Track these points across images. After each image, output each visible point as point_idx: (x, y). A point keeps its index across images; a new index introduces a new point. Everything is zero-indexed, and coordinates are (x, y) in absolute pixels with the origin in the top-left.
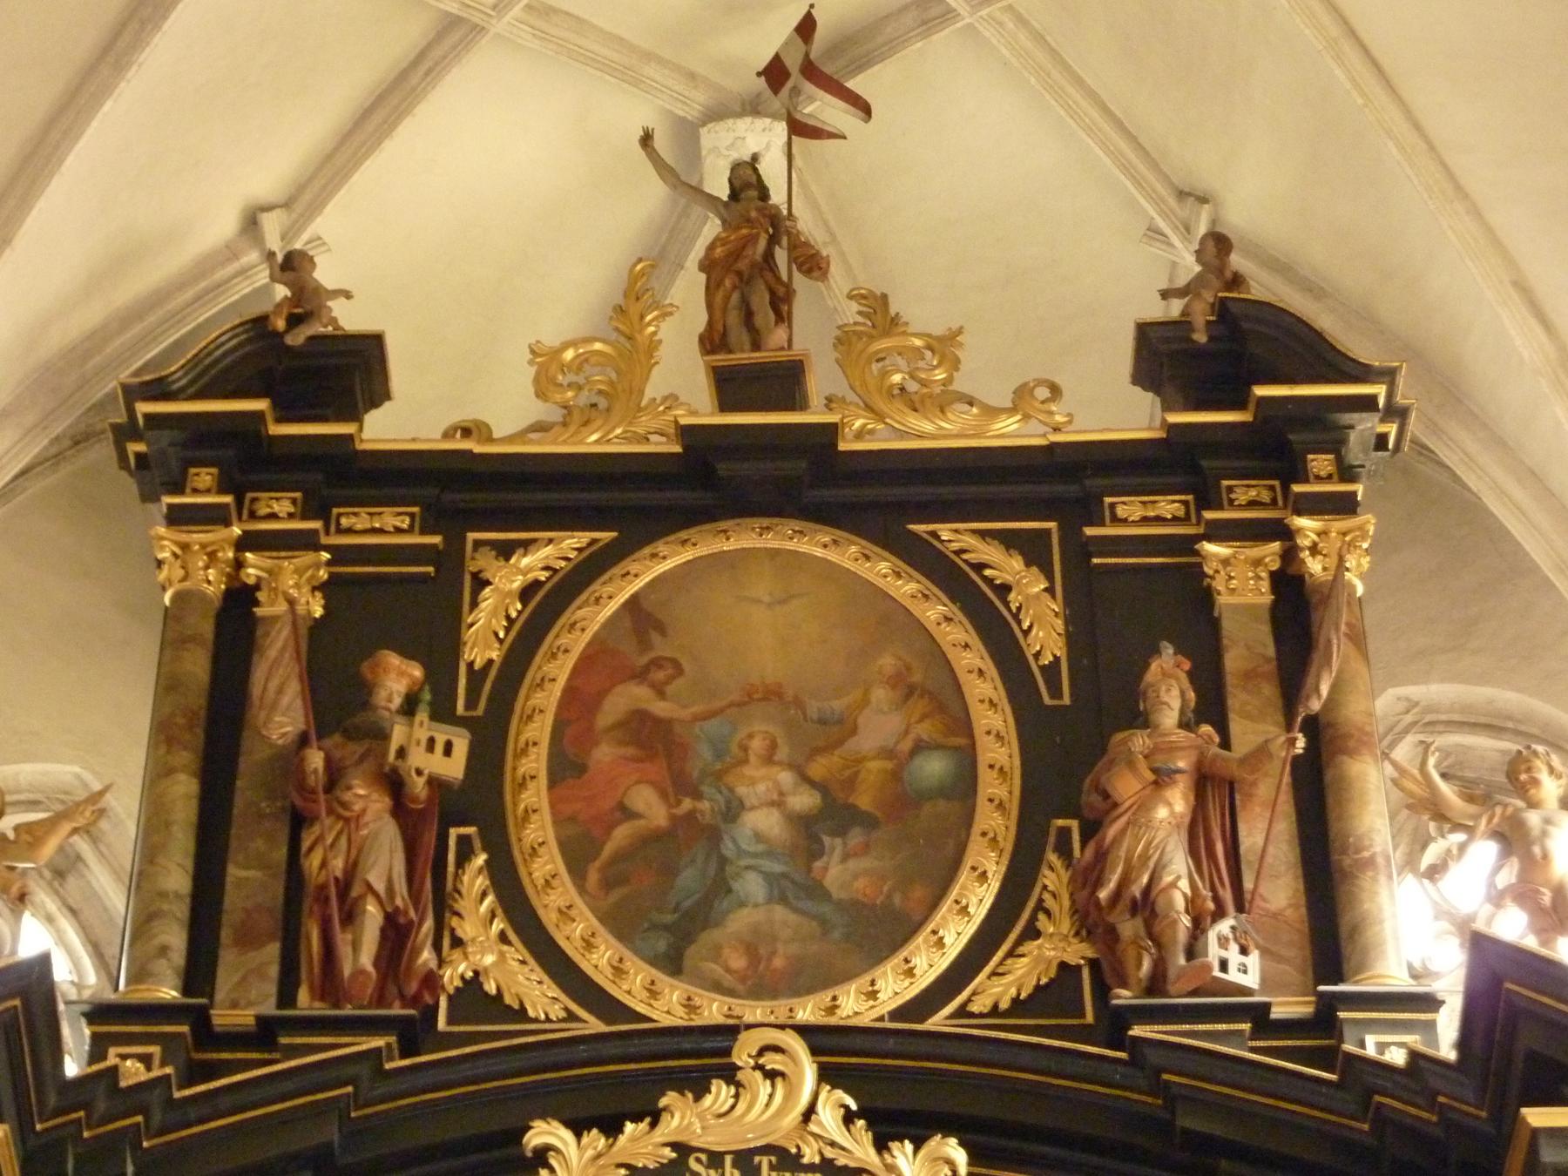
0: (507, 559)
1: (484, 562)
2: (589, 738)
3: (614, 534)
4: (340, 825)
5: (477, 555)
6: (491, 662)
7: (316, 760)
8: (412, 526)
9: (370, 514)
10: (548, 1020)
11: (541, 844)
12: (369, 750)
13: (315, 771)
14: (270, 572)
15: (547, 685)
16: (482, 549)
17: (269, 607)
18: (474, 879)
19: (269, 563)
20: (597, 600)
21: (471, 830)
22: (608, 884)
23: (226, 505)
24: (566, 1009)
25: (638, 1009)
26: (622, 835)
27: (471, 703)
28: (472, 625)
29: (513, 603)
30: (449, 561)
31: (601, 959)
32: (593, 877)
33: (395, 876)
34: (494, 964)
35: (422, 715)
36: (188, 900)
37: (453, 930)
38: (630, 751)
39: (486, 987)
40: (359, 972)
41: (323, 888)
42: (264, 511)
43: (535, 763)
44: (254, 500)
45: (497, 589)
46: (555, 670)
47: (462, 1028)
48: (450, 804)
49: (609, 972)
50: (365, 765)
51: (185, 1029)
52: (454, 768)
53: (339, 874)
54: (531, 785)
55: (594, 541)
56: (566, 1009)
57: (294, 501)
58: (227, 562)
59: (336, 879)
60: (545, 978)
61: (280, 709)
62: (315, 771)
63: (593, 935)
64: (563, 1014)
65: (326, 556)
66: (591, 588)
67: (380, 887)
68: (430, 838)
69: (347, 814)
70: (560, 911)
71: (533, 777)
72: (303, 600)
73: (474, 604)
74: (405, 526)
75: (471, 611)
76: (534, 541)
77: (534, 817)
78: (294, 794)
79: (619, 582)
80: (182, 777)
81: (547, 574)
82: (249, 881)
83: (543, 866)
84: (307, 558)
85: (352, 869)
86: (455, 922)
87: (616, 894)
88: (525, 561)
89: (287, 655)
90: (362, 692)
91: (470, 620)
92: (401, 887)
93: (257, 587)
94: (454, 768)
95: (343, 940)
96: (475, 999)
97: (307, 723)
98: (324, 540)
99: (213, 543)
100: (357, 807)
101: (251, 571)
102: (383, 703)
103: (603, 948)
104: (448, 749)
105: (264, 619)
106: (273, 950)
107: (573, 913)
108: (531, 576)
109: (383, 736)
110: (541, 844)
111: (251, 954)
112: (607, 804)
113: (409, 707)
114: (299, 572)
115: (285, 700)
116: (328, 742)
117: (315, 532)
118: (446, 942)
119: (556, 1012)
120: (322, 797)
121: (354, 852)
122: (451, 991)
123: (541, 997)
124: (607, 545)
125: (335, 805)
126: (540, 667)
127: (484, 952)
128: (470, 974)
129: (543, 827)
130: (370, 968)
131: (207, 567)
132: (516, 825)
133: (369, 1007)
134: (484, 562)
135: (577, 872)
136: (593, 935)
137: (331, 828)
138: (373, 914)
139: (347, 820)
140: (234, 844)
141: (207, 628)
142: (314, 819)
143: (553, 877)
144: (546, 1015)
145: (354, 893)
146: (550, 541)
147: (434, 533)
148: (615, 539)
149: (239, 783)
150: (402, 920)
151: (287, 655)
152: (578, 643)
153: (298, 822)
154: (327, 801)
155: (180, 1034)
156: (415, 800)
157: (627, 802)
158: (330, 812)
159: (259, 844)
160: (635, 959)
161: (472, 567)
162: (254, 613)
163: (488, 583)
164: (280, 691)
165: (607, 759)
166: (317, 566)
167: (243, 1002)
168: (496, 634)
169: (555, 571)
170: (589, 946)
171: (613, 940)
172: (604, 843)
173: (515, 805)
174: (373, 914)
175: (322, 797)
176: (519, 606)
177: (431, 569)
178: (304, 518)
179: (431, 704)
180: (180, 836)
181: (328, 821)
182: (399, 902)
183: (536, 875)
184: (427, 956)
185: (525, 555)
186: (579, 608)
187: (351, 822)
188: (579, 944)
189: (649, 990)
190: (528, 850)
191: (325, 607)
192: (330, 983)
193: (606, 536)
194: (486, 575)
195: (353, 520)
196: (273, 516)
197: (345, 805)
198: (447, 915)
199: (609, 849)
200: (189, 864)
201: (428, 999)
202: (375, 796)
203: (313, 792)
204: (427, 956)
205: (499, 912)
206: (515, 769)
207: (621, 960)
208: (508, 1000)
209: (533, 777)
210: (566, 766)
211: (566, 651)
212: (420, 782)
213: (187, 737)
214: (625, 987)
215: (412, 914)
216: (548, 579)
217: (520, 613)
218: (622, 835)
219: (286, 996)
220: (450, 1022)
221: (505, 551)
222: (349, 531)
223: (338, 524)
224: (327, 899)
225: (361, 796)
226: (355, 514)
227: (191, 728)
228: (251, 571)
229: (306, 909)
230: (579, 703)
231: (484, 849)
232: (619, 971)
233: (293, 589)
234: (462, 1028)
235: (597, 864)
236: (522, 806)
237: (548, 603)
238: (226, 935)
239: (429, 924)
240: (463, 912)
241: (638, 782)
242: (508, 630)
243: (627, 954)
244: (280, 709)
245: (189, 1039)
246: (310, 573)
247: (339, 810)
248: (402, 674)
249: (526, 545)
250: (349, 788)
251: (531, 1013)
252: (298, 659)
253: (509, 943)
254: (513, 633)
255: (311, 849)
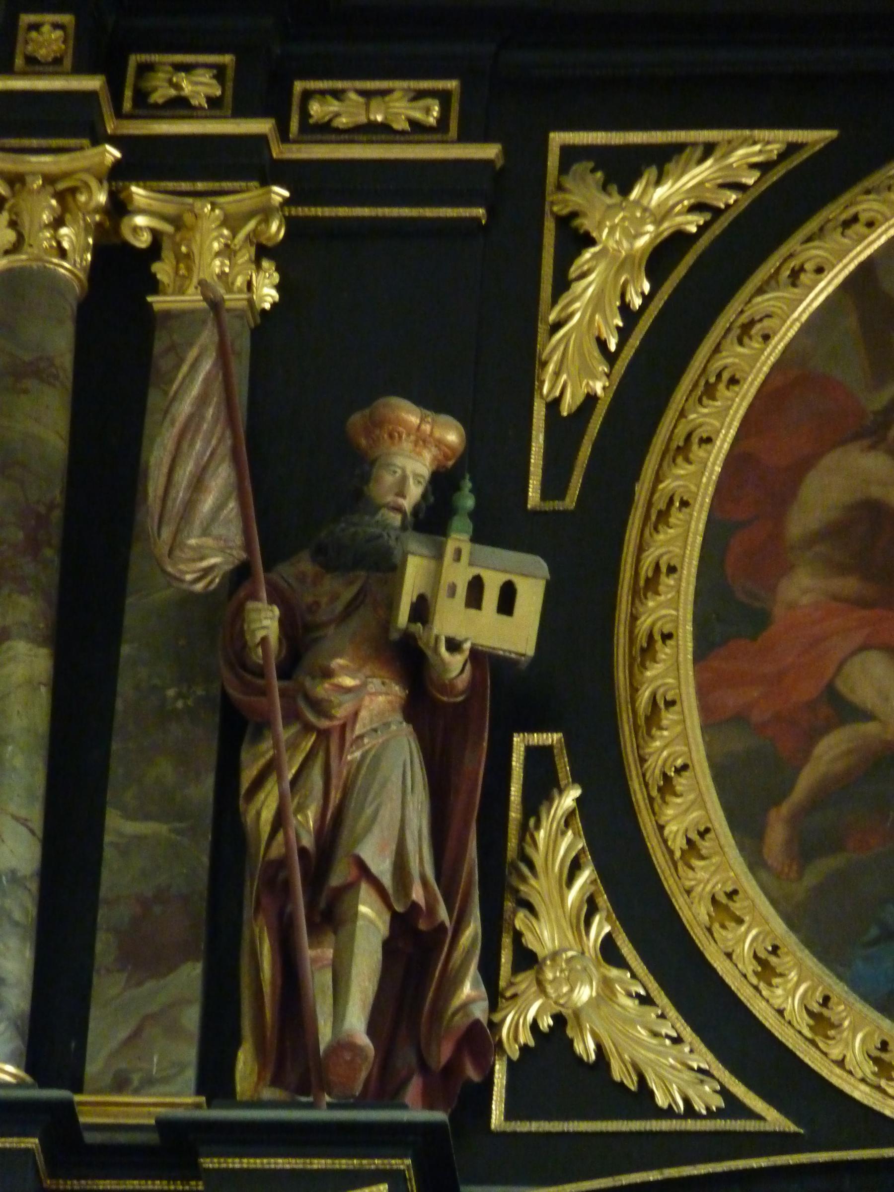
0: (625, 191)
1: (583, 195)
2: (772, 560)
3: (830, 134)
4: (308, 743)
5: (568, 182)
6: (591, 399)
7: (265, 622)
8: (443, 120)
9: (367, 94)
10: (690, 1112)
11: (679, 771)
12: (362, 594)
13: (264, 641)
14: (177, 221)
15: (697, 452)
16: (582, 167)
17: (174, 296)
18: (556, 837)
19: (170, 207)
20: (795, 274)
21: (552, 738)
22: (806, 848)
23: (91, 96)
24: (724, 1092)
25: (857, 1095)
26: (831, 751)
27: (554, 485)
28: (557, 326)
29: (635, 280)
30: (515, 191)
31: (787, 999)
32: (777, 834)
33: (411, 846)
34: (595, 1002)
35: (459, 539)
36: (34, 886)
37: (518, 936)
38: (850, 585)
39: (579, 1048)
40: (343, 1046)
41: (282, 863)
42: (161, 94)
43: (672, 609)
44: (145, 69)
45: (604, 251)
46: (714, 422)
47: (534, 1126)
48: (510, 692)
49: (803, 1022)
50: (354, 623)
51: (32, 1143)
52: (517, 635)
53: (308, 841)
54: (664, 652)
55: (792, 148)
56: (724, 1092)
57: (220, 73)
58: (98, 209)
59: (303, 851)
60: (687, 1033)
61: (198, 518)
62: (264, 641)
63: (775, 950)
64: (718, 1102)
65: (280, 193)
66: (784, 250)
67: (381, 866)
68: (476, 763)
69: (324, 724)
70: (714, 900)
71: (667, 637)
72: (240, 281)
73: (562, 284)
74: (432, 120)
75: (554, 301)
76: (679, 148)
77: (668, 717)
78: (226, 673)
79: (836, 239)
80: (21, 647)
81: (700, 219)
82: (144, 843)
83: (685, 813)
84: (249, 196)
85: (331, 832)
86: (521, 920)
87: (824, 867)
88: (660, 193)
89: (210, 412)
90: (352, 472)
91: (552, 317)
92: (421, 859)
93: (155, 251)
94: (517, 635)
95: (317, 956)
96: (556, 1068)
97: (248, 546)
98: (278, 151)
99: (66, 175)
100: (341, 713)
101: (140, 221)
102: (390, 498)
103: (793, 976)
104: (507, 600)
105: (168, 315)
106: (191, 975)
107: (737, 907)
108: (668, 227)
109: (390, 568)
110: (679, 771)
111: (150, 985)
112: (808, 689)
113: (432, 520)
114: (232, 222)
115: (208, 503)
116: (286, 571)
117: (261, 140)
118: (506, 958)
119: (705, 1097)
120: (276, 684)
121: (335, 797)
122: (515, 1055)
123: (678, 1071)
124: (821, 152)
125: (302, 704)
126: (682, 414)
127: (577, 982)
128: (546, 1022)
129: (684, 736)
130: (363, 1040)
131: (58, 223)
132: (636, 728)
133: (359, 1103)
134: (583, 195)
135: (746, 824)
136: (775, 950)
137: (293, 746)
138: (369, 914)
139: (324, 735)
140: (117, 771)
141: (60, 343)
142: (263, 726)
143: (703, 834)
144: (687, 1101)
145: (336, 880)
146: (709, 149)
147: (485, 138)
148: (831, 145)
149: (126, 650)
150: (422, 926)
151: (210, 412)
152: (757, 363)
153: (236, 727)
154: (283, 694)
155: (27, 1152)
156: (448, 688)
157: (841, 686)
158: (292, 715)
159: (164, 770)
160: (853, 998)
161: (558, 204)
162: (150, 305)
163: (588, 241)
164: (198, 484)
165: (805, 600)
166: (265, 213)
167: (136, 1079)
168: (602, 344)
169: (717, 212)
170: (766, 970)
171: (810, 961)
172: (798, 770)
173: (634, 690)
174: (369, 914)
175: (276, 684)
176: (647, 287)
177: (480, 212)
178: (240, 111)
179: (474, 515)
180: (19, 762)
181: (285, 734)
182: (417, 894)
183: (671, 828)
184: (469, 989)
185: (658, 182)
186: (760, 291)
187: (330, 739)
188: (750, 967)
189: (877, 1061)
190: (655, 780)
191: (279, 288)
192: (294, 1054)
193: (815, 137)
194: (586, 224)
195: (334, 106)
196: (179, 106)
197: (320, 707)
198: (509, 905)
199: (806, 780)
200: (36, 814)
201: (472, 1073)
202: (375, 684)
203: (260, 672)
204: (469, 989)
205: (603, 900)
206: (634, 618)
207: (826, 1000)
208: (618, 1072)
209: (667, 637)
210: (728, 616)
211: (733, 381)
212: (455, 665)
213: (29, 567)
214: (836, 1053)
215: (443, 914)
216: (702, 229)
217: (647, 299)
218: (831, 751)
219: (215, 1079)
220: (510, 1115)
221: (623, 171)
222: (325, 131)
223: (305, 114)
224: (286, 888)
225: (348, 690)
226: (338, 95)
227: (33, 546)
228: (140, 221)
229: (252, 900)
230: (755, 482)
231: (577, 778)
232: (821, 1023)
233: (223, 260)
234: (534, 1126)
235: (785, 809)
236: (645, 695)
237: (703, 277)
238: (104, 945)
239: (473, 929)
240: (535, 900)
241: (864, 647)
242: (624, 334)
243: (839, 989)
244: (198, 518)
245: (40, 1159)
246: (251, 225)
247: (305, 708)
248: (422, 440)
249: (662, 159)
250: (327, 674)
251: (661, 1100)
252: (231, 421)
253: (619, 961)
254: (635, 341)
255: (258, 783)
